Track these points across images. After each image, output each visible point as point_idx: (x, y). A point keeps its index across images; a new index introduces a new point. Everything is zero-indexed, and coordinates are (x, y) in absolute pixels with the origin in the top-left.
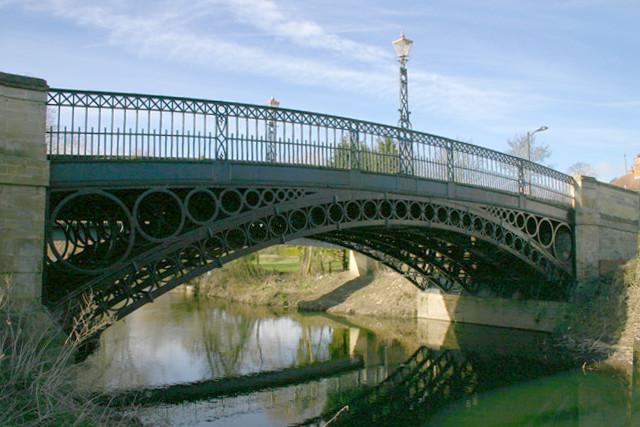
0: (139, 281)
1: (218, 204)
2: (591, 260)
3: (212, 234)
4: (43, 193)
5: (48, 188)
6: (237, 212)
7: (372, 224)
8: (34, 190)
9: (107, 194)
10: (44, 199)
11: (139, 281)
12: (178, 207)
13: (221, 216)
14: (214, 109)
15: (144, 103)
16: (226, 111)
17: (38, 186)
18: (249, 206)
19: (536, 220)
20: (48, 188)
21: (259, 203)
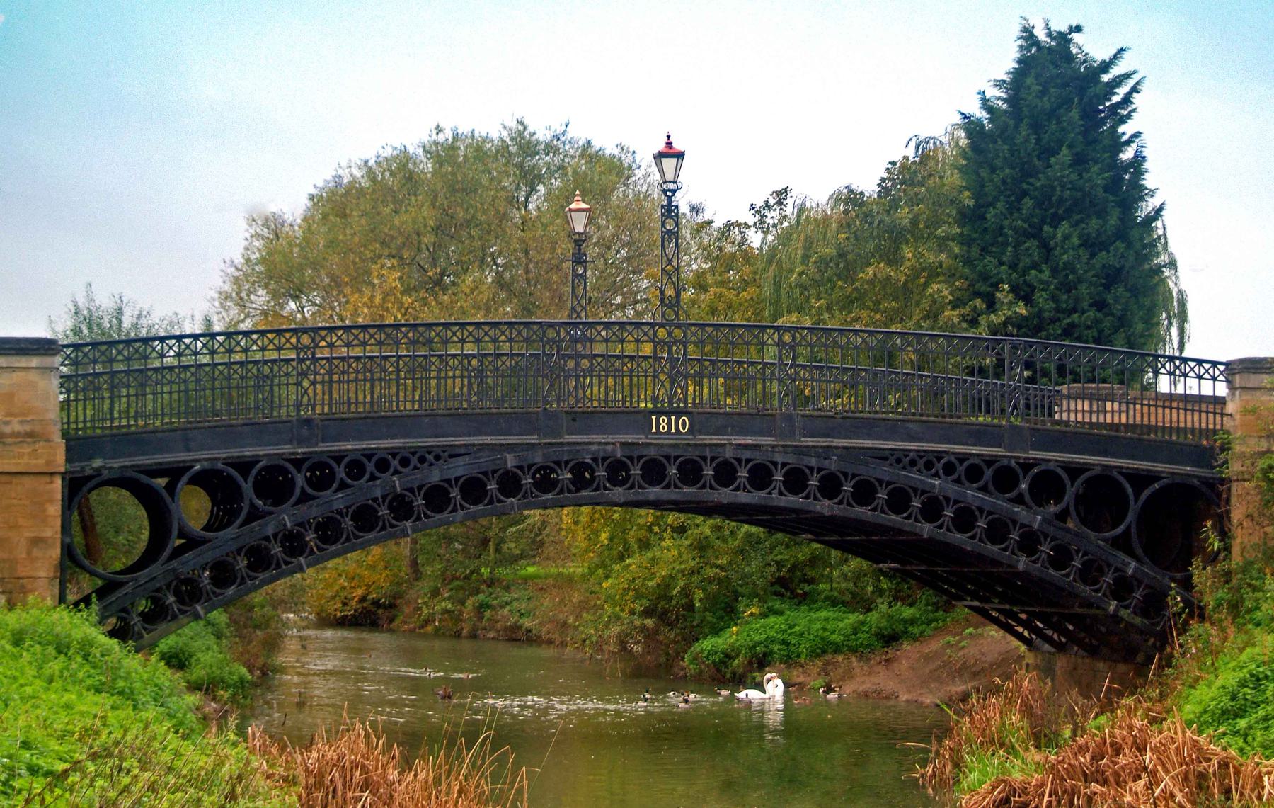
0: (1026, 633)
1: (300, 480)
2: (541, 139)
3: (289, 525)
4: (58, 482)
5: (63, 475)
6: (328, 492)
7: (890, 520)
8: (47, 479)
9: (1059, 471)
10: (60, 487)
11: (1026, 633)
12: (239, 487)
13: (304, 498)
14: (293, 340)
15: (646, 334)
16: (313, 340)
17: (52, 474)
18: (377, 474)
19: (963, 478)
20: (63, 475)
21: (966, 464)
